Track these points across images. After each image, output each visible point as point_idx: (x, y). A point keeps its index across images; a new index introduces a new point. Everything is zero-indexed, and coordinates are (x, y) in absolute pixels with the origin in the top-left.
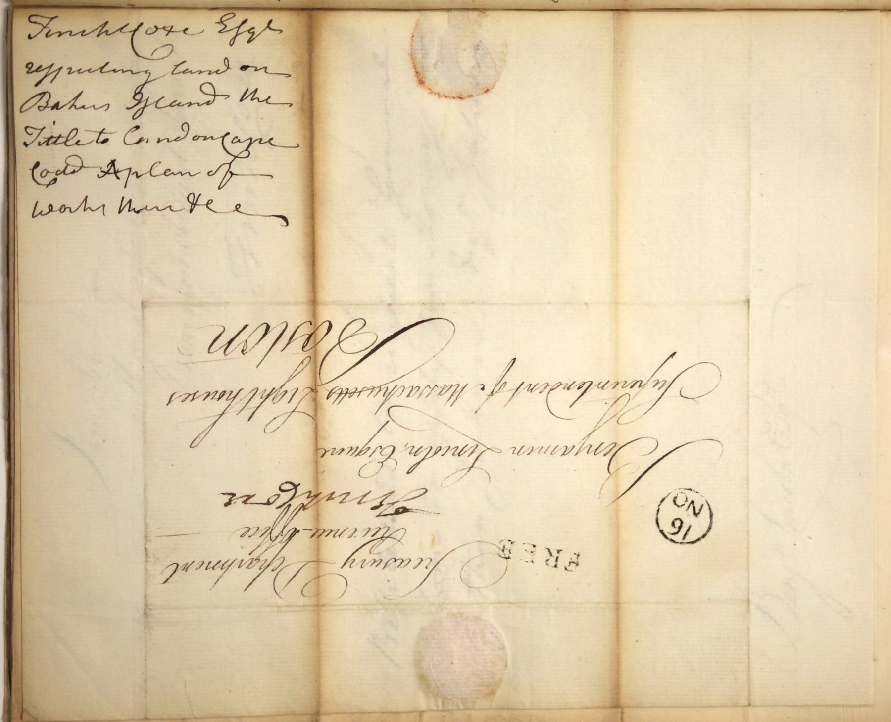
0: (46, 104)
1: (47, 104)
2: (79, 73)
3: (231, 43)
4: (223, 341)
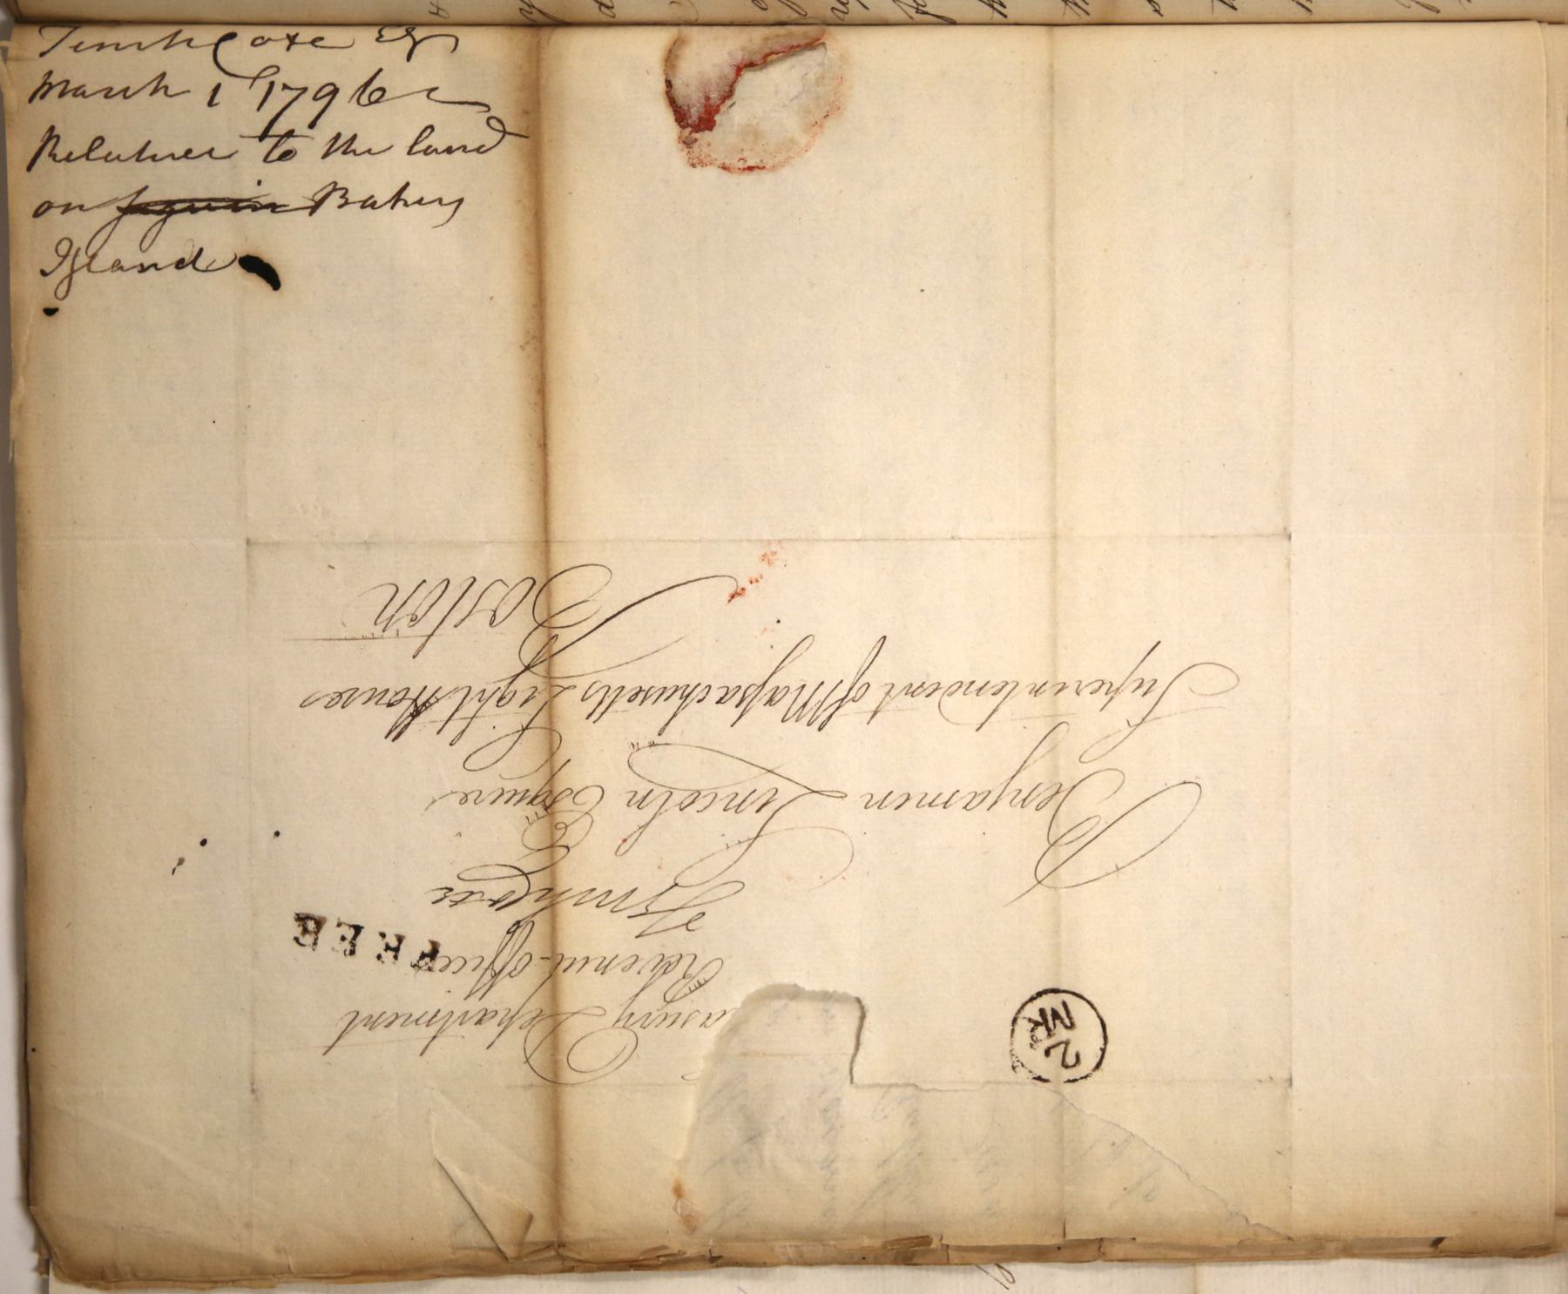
0: (383, 33)
1: (380, 32)
2: (125, 97)
3: (429, 130)
4: (680, 1022)
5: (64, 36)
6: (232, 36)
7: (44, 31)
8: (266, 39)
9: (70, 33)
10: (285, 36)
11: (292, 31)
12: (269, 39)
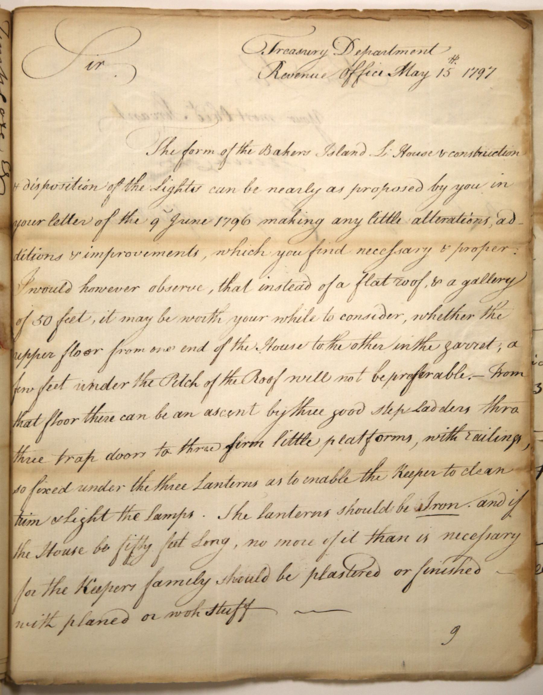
0: (6, 164)
1: (7, 162)
5: (4, 31)
6: (5, 100)
7: (7, 23)
8: (3, 115)
9: (6, 34)
10: (4, 122)
11: (7, 125)
12: (3, 116)
